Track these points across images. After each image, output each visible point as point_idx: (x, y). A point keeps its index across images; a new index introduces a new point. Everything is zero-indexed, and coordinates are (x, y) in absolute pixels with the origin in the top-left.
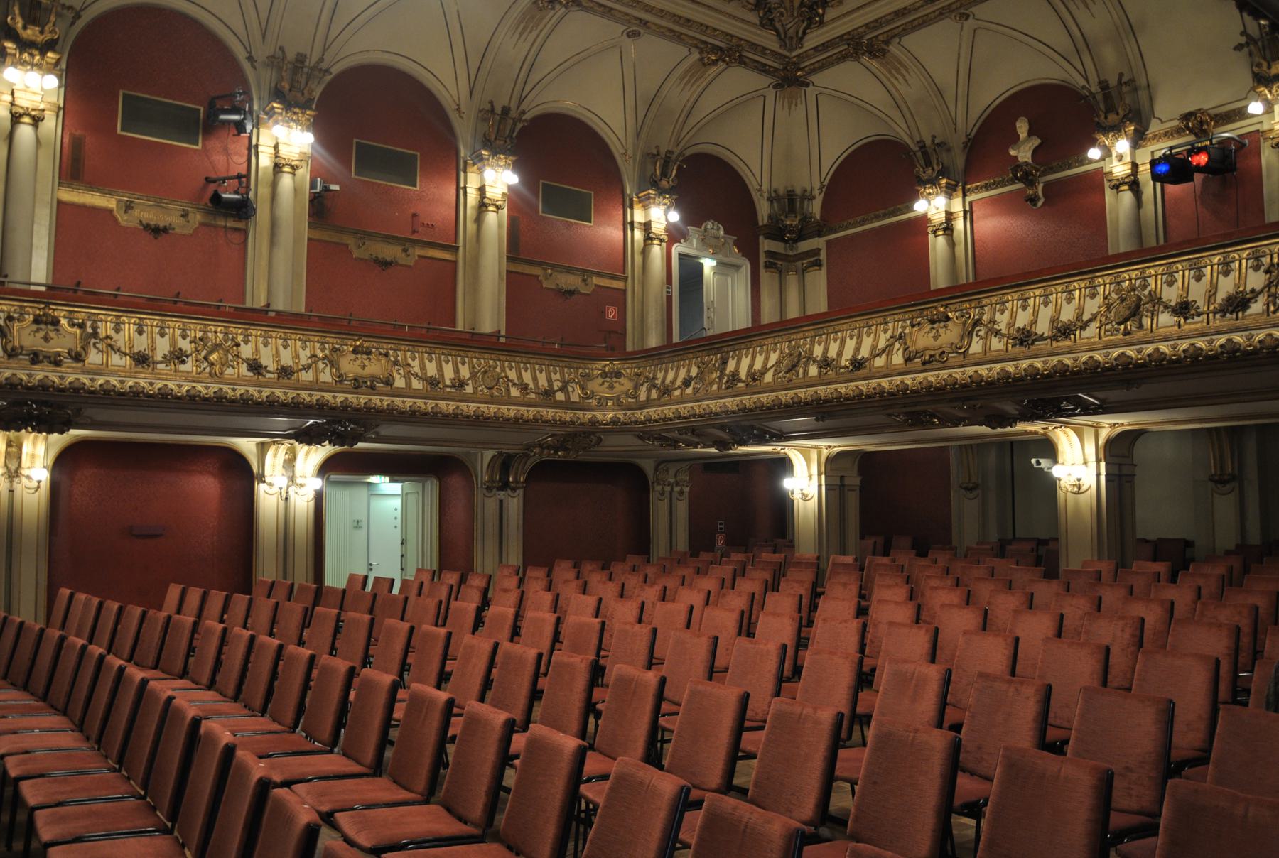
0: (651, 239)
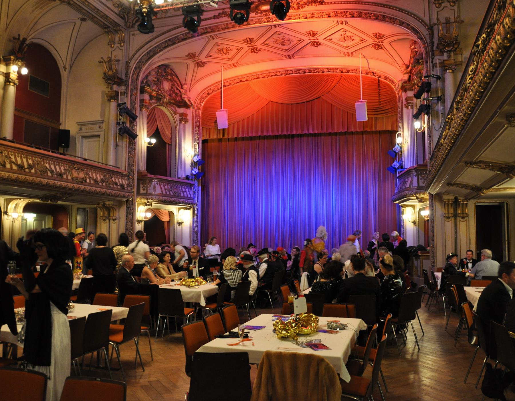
0: (10, 82)
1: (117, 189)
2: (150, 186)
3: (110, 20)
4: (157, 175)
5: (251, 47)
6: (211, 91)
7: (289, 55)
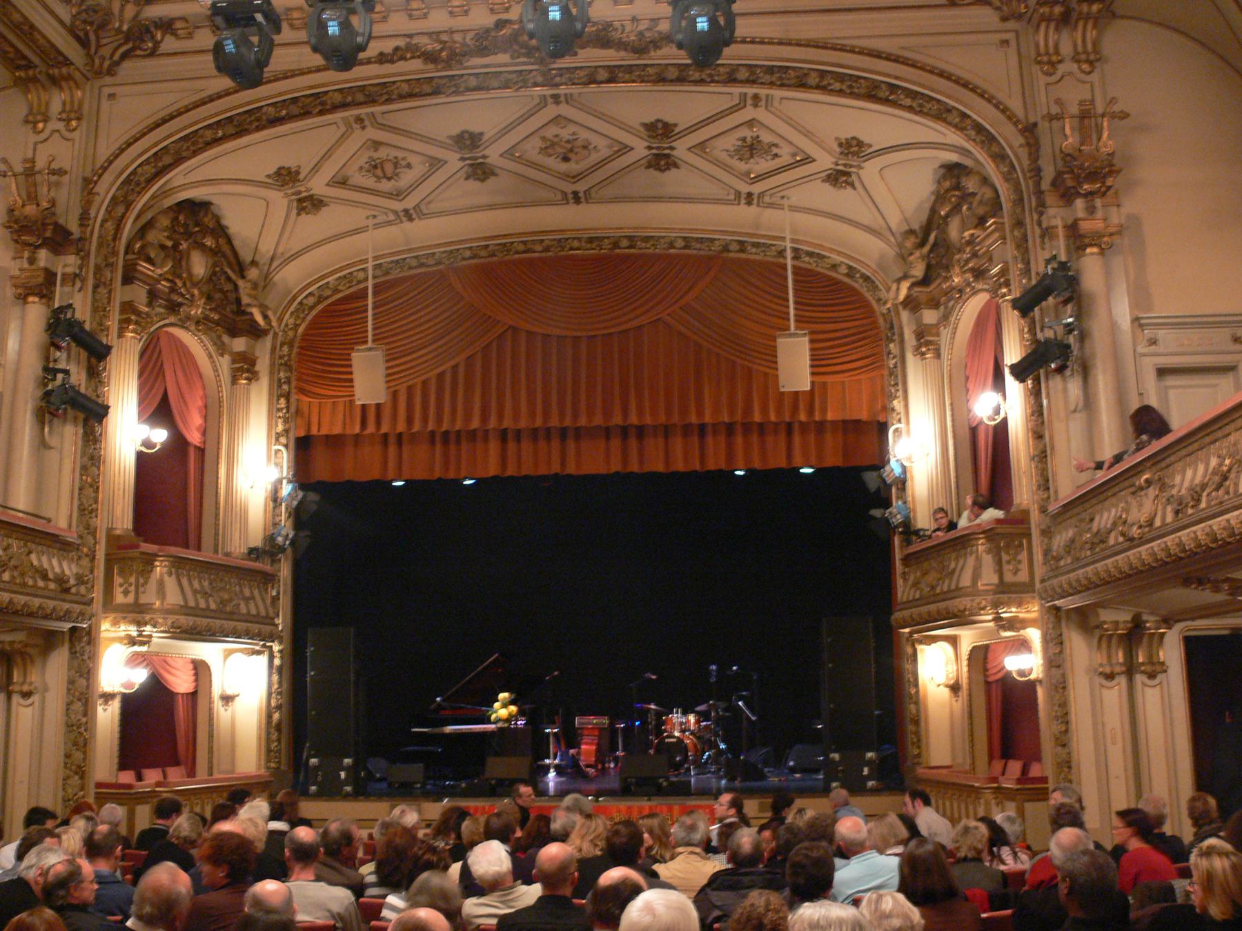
1: (47, 593)
2: (146, 583)
3: (42, 41)
4: (170, 545)
5: (468, 162)
6: (327, 293)
7: (575, 194)
